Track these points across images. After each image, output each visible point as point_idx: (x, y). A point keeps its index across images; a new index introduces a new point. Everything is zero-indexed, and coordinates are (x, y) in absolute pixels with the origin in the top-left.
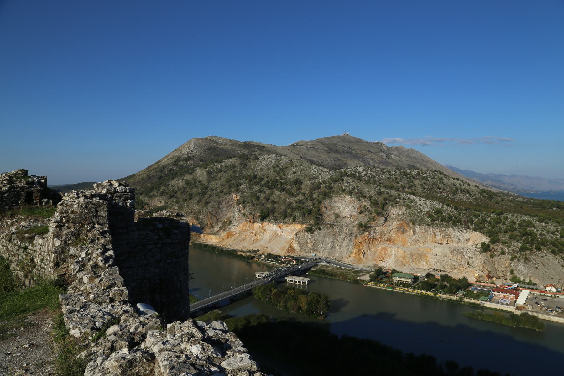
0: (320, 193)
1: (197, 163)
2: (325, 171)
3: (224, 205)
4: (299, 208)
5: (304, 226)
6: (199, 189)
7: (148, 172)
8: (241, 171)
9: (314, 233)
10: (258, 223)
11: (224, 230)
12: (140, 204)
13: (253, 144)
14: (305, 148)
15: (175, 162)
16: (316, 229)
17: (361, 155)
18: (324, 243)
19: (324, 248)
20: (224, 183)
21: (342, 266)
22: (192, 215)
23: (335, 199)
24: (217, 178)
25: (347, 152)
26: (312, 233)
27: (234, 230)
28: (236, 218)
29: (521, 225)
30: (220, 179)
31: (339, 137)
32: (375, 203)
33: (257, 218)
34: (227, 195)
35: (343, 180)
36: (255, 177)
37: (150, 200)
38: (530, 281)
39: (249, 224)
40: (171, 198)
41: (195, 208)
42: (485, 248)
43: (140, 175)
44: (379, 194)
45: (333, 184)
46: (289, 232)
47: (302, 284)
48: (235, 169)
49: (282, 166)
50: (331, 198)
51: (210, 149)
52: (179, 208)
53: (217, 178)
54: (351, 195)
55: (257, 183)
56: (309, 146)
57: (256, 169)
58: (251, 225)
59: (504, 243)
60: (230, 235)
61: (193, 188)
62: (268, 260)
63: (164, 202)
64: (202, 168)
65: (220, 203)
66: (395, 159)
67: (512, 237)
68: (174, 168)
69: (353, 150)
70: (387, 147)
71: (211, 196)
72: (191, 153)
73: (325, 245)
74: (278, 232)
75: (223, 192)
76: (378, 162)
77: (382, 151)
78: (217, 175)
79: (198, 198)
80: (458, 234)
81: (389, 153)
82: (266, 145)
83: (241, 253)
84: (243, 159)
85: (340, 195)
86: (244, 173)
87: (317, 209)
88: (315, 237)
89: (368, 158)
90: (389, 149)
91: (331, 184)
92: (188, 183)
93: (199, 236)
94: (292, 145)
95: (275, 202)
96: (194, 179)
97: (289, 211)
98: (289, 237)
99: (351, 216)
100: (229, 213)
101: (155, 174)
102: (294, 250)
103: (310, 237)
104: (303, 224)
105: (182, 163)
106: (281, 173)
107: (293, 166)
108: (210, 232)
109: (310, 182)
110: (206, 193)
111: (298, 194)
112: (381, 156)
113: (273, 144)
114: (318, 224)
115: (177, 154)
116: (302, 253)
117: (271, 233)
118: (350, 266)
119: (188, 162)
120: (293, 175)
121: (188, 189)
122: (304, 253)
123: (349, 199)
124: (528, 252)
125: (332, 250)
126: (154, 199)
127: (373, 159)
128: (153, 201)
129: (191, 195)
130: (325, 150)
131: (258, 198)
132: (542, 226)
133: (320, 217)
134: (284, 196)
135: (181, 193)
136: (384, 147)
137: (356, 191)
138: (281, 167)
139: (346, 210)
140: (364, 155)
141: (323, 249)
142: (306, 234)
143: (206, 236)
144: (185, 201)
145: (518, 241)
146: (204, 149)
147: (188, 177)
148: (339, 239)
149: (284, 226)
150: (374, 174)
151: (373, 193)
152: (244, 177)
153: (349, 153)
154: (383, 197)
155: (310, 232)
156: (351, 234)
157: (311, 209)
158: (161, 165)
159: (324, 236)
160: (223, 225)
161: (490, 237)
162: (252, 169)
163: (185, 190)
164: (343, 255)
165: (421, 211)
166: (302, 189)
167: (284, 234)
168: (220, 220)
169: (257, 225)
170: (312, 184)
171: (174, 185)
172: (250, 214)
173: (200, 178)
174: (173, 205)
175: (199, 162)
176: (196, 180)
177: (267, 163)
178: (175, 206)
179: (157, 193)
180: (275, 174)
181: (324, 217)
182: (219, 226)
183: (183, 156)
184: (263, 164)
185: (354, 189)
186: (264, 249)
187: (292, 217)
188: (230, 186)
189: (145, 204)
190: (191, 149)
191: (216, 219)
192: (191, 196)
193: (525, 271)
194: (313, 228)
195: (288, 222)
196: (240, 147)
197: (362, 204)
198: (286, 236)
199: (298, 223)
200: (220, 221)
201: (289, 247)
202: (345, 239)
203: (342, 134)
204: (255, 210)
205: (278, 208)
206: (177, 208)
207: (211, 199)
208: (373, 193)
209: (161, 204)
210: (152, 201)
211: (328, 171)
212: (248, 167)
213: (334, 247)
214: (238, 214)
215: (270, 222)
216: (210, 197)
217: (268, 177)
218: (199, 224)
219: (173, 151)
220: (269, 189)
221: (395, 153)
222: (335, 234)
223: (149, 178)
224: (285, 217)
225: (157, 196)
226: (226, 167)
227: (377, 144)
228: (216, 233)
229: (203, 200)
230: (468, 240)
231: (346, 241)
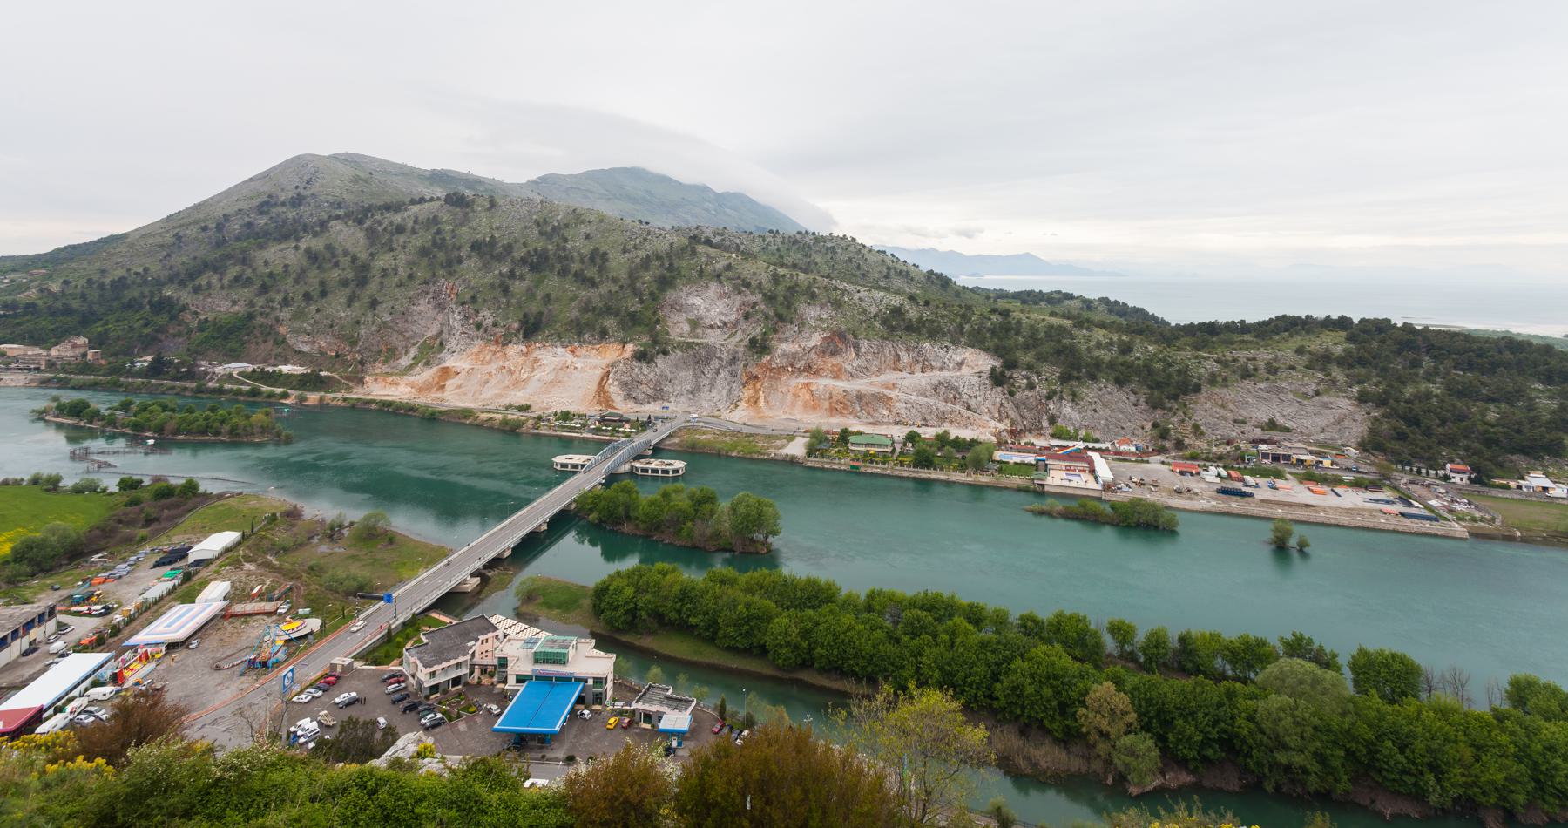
11: (428, 364)
16: (658, 353)
29: (1048, 335)
32: (770, 298)
38: (1087, 434)
42: (997, 379)
55: (499, 258)
59: (1029, 368)
67: (1041, 358)
79: (347, 292)
80: (942, 353)
92: (312, 256)
96: (329, 247)
99: (725, 324)
101: (203, 234)
103: (646, 370)
105: (281, 209)
115: (265, 188)
124: (1073, 383)
132: (1085, 336)
145: (1053, 364)
148: (706, 372)
151: (764, 278)
161: (1001, 356)
165: (865, 311)
170: (631, 260)
182: (412, 355)
193: (1076, 416)
200: (414, 344)
206: (288, 316)
208: (764, 278)
209: (236, 308)
214: (462, 326)
230: (960, 364)
231: (722, 376)
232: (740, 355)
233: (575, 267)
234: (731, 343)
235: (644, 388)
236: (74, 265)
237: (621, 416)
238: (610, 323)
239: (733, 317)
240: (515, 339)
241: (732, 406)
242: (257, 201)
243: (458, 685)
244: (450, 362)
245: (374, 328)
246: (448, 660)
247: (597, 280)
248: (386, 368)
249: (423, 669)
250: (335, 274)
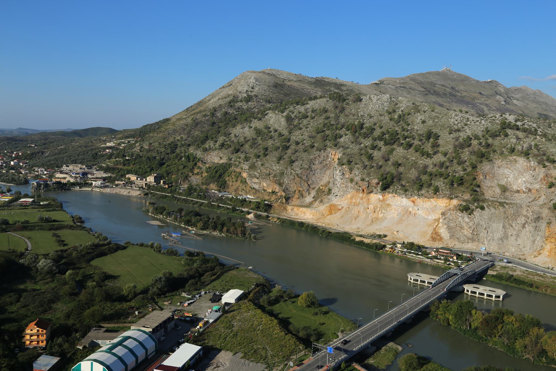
0: (472, 153)
1: (262, 105)
2: (473, 120)
3: (317, 166)
4: (441, 175)
5: (455, 202)
6: (277, 141)
7: (191, 115)
8: (337, 117)
9: (473, 214)
10: (376, 193)
11: (321, 201)
12: (191, 160)
13: (327, 80)
14: (393, 87)
15: (231, 103)
16: (477, 208)
17: (469, 99)
18: (490, 230)
19: (489, 238)
20: (314, 134)
21: (539, 270)
22: (271, 179)
23: (498, 162)
24: (301, 126)
25: (451, 94)
26: (470, 214)
27: (337, 202)
28: (338, 185)
30: (307, 128)
31: (438, 73)
33: (373, 186)
34: (320, 151)
35: (506, 135)
36: (361, 126)
37: (206, 155)
39: (361, 195)
40: (236, 153)
41: (275, 168)
43: (179, 120)
45: (490, 141)
46: (429, 209)
47: (493, 299)
48: (329, 114)
49: (402, 111)
50: (491, 160)
51: (276, 86)
52: (250, 167)
53: (301, 126)
54: (528, 158)
55: (366, 136)
56: (398, 86)
57: (360, 115)
58: (364, 196)
60: (333, 209)
61: (267, 140)
62: (410, 253)
63: (225, 158)
64: (276, 112)
65: (311, 162)
66: (519, 105)
68: (231, 111)
69: (458, 91)
70: (505, 89)
71: (296, 152)
72: (251, 92)
73: (492, 232)
74: (411, 209)
75: (313, 147)
76: (495, 108)
77: (497, 94)
78: (300, 121)
79: (277, 154)
81: (507, 97)
82: (345, 82)
83: (362, 239)
84: (337, 99)
85: (506, 157)
86: (342, 120)
87: (471, 178)
88: (476, 221)
89: (481, 104)
90: (507, 91)
91: (487, 139)
92: (258, 132)
93: (285, 209)
94: (374, 84)
95: (400, 165)
96: (268, 128)
97: (424, 178)
98: (430, 218)
99: (530, 190)
100: (324, 178)
101: (204, 119)
102: (441, 239)
103: (467, 219)
104: (452, 199)
105: (240, 104)
106: (401, 122)
107: (419, 112)
108: (300, 203)
109: (451, 135)
110: (289, 147)
111: (435, 153)
112: (498, 101)
113: (355, 82)
114: (478, 200)
115: (230, 92)
116: (453, 244)
117: (400, 211)
118: (547, 270)
119: (250, 103)
120: (421, 125)
121: (261, 142)
122: (457, 243)
123: (525, 164)
125: (503, 241)
126: (211, 154)
127: (487, 105)
128: (209, 156)
129: (266, 149)
130: (420, 91)
131: (371, 158)
133: (478, 189)
134: (412, 155)
135: (250, 146)
136: (500, 88)
137: (536, 152)
138: (400, 113)
139: (520, 181)
140: (474, 99)
141: (489, 238)
142: (460, 215)
143: (296, 209)
144: (259, 158)
146: (269, 86)
147: (256, 124)
148: (514, 225)
149: (419, 201)
150: (535, 125)
152: (343, 126)
153: (453, 95)
155: (466, 212)
156: (538, 219)
157: (462, 176)
158: (211, 107)
159: (490, 219)
160: (317, 193)
162: (354, 115)
163: (256, 142)
164: (523, 249)
166: (440, 146)
167: (420, 212)
168: (312, 187)
169: (376, 197)
170: (457, 139)
171: (237, 135)
172: (363, 180)
173: (276, 126)
174: (240, 162)
175: (264, 103)
176: (270, 128)
177: (377, 106)
178: (244, 164)
179: (215, 145)
180: (392, 123)
181: (483, 189)
182: (312, 195)
183: (240, 95)
184: (370, 108)
185: (531, 149)
186: (393, 233)
187: (432, 188)
188: (325, 138)
189: (199, 160)
190: (250, 85)
191: (307, 185)
192: (266, 151)
194: (470, 205)
195: (426, 194)
196: (310, 84)
197: (549, 172)
198: (424, 215)
199: (442, 198)
200: (314, 189)
201: (432, 233)
202: (526, 226)
203: (442, 68)
204: (369, 174)
205: (406, 173)
206: (247, 167)
207: (298, 157)
209: (222, 161)
210: (207, 155)
211: (478, 119)
212: (346, 112)
213: (505, 237)
214: (342, 179)
215: (396, 194)
216: (295, 154)
217: (382, 127)
218: (284, 191)
219: (220, 89)
220: (386, 144)
221: (517, 96)
222: (507, 217)
223: (196, 123)
224: (421, 187)
225: (216, 149)
226: (313, 111)
227: (491, 84)
228: (309, 206)
229: (285, 157)
231: (527, 229)
233: (416, 142)
236: (151, 135)
238: (439, 183)
240: (375, 190)
241: (535, 253)
242: (228, 100)
244: (335, 201)
245: (292, 177)
250: (270, 143)
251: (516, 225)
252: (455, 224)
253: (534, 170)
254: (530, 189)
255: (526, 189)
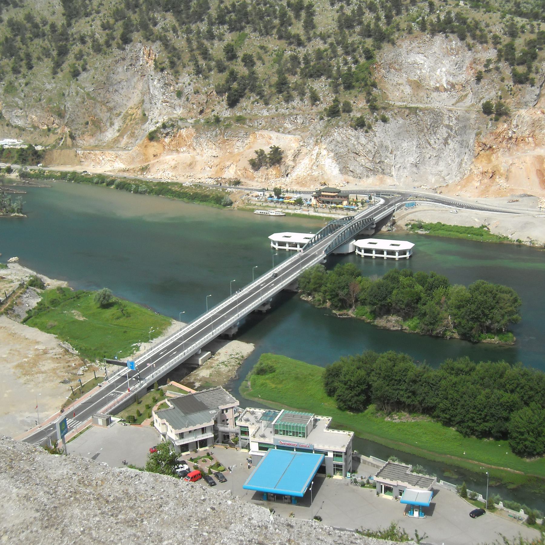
9: (373, 131)
26: (367, 132)
44: (513, 33)
99: (453, 86)
103: (363, 140)
111: (309, 39)
148: (432, 142)
151: (498, 29)
154: (525, 40)
182: (116, 127)
202: (449, 141)
208: (498, 29)
224: (359, 111)
231: (451, 146)
232: (472, 121)
234: (460, 109)
235: (362, 160)
237: (339, 192)
239: (462, 78)
243: (206, 446)
246: (194, 425)
247: (303, 38)
248: (92, 141)
249: (173, 430)
251: (435, 142)
252: (346, 149)
253: (457, 54)
254: (452, 84)
255: (447, 84)
